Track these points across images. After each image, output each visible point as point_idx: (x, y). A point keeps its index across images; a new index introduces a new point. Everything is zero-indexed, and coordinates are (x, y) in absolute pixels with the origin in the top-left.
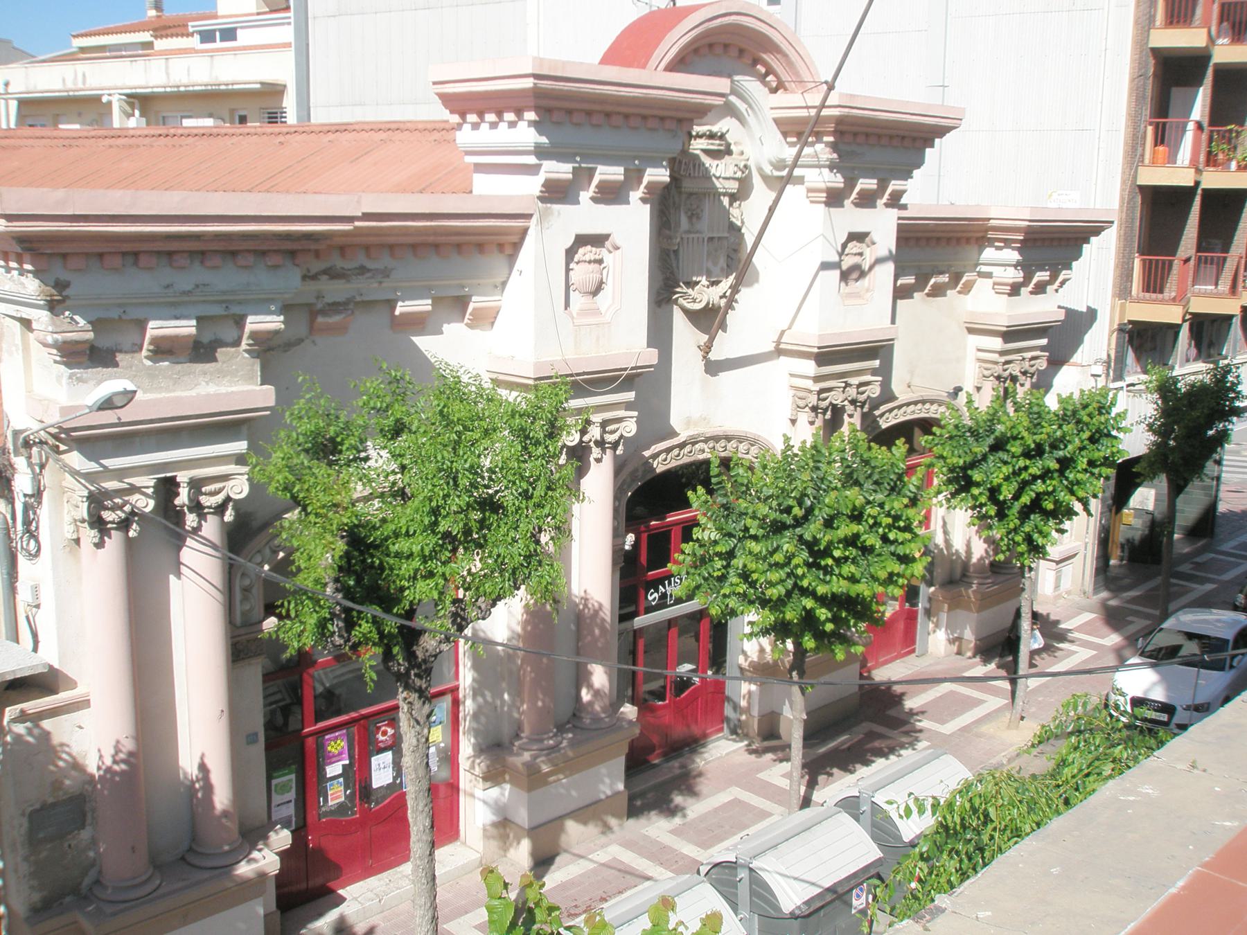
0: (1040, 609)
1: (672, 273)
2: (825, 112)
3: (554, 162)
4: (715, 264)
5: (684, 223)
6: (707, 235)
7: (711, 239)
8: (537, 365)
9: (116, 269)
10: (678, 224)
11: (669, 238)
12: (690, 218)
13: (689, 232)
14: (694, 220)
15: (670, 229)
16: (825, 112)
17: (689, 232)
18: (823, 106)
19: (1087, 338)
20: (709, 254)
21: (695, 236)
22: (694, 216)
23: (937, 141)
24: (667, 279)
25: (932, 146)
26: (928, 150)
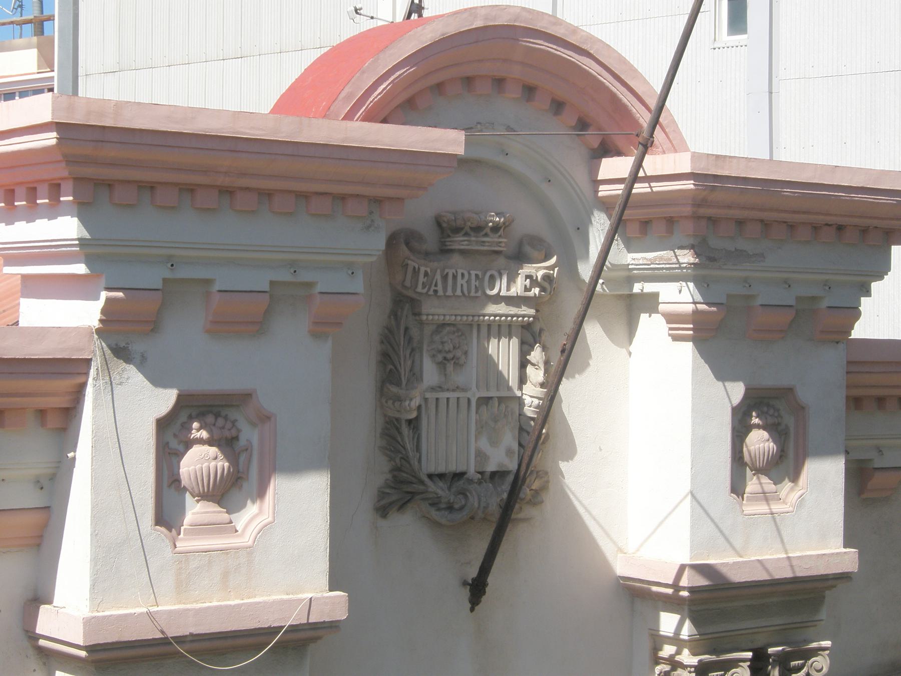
0: (432, 469)
1: (406, 459)
2: (640, 188)
3: (23, 224)
4: (494, 443)
5: (430, 373)
6: (475, 394)
7: (485, 401)
8: (90, 624)
9: (173, 208)
10: (416, 376)
11: (398, 399)
12: (442, 366)
13: (440, 388)
14: (450, 367)
15: (398, 384)
16: (640, 188)
17: (440, 388)
18: (634, 178)
19: (38, 221)
20: (481, 427)
21: (453, 395)
22: (449, 361)
23: (875, 286)
24: (396, 469)
25: (868, 293)
26: (863, 300)
